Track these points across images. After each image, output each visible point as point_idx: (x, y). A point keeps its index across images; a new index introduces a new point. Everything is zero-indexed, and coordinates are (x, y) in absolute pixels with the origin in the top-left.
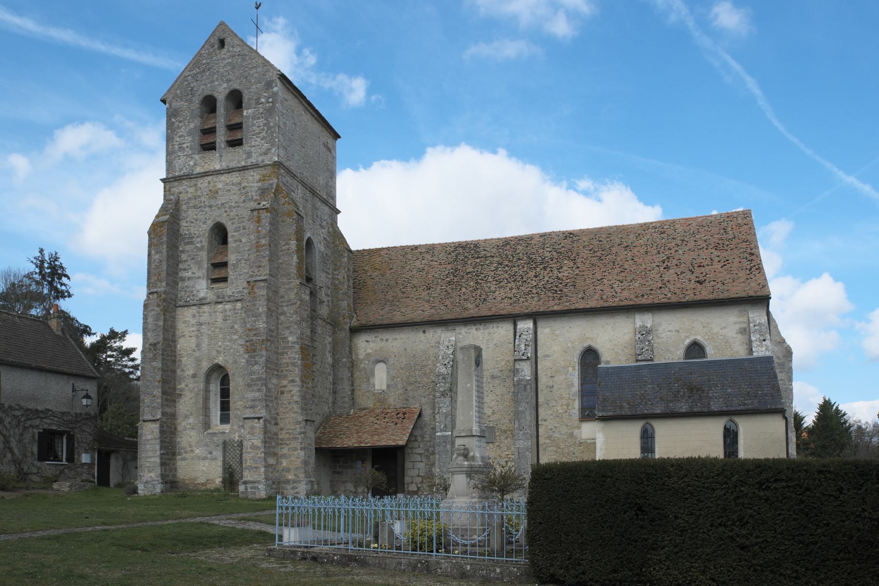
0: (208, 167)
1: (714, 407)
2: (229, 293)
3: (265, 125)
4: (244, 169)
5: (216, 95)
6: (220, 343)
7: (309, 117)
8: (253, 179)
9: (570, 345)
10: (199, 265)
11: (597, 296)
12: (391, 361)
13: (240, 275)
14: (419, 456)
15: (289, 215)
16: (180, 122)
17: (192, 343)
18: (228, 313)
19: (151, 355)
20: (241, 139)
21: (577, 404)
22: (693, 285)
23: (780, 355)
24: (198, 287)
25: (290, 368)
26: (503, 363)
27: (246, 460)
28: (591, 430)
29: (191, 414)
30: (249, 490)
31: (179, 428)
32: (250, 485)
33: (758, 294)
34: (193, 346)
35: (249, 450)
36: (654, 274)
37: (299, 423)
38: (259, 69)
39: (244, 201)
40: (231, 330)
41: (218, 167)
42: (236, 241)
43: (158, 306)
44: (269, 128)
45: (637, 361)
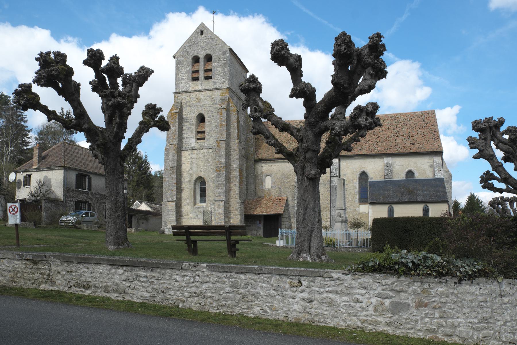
1: (419, 200)
2: (206, 145)
3: (222, 70)
4: (213, 90)
5: (199, 56)
7: (238, 65)
8: (217, 95)
10: (191, 132)
11: (367, 149)
12: (273, 175)
15: (234, 111)
18: (206, 154)
19: (171, 172)
20: (211, 76)
21: (358, 197)
22: (409, 145)
23: (447, 177)
24: (191, 142)
25: (234, 179)
28: (364, 208)
31: (183, 205)
33: (438, 150)
34: (189, 168)
36: (392, 139)
37: (238, 203)
38: (220, 46)
41: (200, 88)
43: (174, 150)
44: (225, 72)
45: (385, 178)
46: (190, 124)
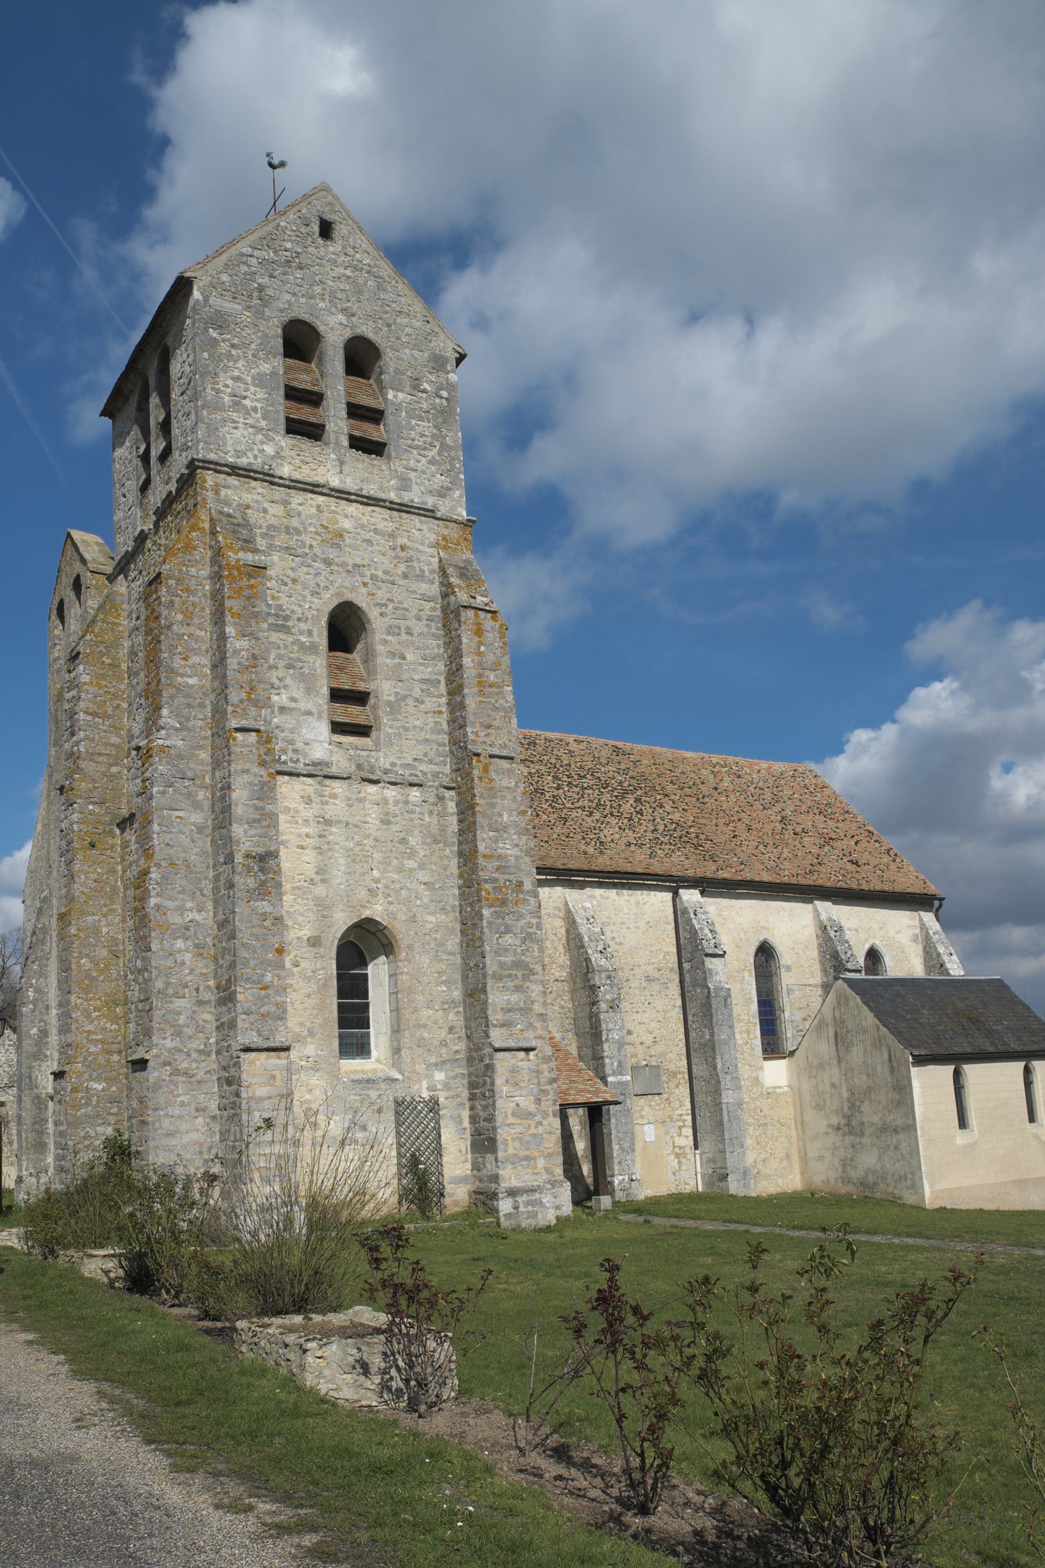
0: (305, 474)
4: (403, 508)
9: (742, 935)
13: (406, 729)
16: (233, 346)
19: (251, 883)
20: (383, 445)
24: (306, 733)
30: (522, 1209)
34: (310, 871)
39: (405, 576)
40: (402, 848)
41: (335, 482)
44: (444, 447)
46: (301, 645)
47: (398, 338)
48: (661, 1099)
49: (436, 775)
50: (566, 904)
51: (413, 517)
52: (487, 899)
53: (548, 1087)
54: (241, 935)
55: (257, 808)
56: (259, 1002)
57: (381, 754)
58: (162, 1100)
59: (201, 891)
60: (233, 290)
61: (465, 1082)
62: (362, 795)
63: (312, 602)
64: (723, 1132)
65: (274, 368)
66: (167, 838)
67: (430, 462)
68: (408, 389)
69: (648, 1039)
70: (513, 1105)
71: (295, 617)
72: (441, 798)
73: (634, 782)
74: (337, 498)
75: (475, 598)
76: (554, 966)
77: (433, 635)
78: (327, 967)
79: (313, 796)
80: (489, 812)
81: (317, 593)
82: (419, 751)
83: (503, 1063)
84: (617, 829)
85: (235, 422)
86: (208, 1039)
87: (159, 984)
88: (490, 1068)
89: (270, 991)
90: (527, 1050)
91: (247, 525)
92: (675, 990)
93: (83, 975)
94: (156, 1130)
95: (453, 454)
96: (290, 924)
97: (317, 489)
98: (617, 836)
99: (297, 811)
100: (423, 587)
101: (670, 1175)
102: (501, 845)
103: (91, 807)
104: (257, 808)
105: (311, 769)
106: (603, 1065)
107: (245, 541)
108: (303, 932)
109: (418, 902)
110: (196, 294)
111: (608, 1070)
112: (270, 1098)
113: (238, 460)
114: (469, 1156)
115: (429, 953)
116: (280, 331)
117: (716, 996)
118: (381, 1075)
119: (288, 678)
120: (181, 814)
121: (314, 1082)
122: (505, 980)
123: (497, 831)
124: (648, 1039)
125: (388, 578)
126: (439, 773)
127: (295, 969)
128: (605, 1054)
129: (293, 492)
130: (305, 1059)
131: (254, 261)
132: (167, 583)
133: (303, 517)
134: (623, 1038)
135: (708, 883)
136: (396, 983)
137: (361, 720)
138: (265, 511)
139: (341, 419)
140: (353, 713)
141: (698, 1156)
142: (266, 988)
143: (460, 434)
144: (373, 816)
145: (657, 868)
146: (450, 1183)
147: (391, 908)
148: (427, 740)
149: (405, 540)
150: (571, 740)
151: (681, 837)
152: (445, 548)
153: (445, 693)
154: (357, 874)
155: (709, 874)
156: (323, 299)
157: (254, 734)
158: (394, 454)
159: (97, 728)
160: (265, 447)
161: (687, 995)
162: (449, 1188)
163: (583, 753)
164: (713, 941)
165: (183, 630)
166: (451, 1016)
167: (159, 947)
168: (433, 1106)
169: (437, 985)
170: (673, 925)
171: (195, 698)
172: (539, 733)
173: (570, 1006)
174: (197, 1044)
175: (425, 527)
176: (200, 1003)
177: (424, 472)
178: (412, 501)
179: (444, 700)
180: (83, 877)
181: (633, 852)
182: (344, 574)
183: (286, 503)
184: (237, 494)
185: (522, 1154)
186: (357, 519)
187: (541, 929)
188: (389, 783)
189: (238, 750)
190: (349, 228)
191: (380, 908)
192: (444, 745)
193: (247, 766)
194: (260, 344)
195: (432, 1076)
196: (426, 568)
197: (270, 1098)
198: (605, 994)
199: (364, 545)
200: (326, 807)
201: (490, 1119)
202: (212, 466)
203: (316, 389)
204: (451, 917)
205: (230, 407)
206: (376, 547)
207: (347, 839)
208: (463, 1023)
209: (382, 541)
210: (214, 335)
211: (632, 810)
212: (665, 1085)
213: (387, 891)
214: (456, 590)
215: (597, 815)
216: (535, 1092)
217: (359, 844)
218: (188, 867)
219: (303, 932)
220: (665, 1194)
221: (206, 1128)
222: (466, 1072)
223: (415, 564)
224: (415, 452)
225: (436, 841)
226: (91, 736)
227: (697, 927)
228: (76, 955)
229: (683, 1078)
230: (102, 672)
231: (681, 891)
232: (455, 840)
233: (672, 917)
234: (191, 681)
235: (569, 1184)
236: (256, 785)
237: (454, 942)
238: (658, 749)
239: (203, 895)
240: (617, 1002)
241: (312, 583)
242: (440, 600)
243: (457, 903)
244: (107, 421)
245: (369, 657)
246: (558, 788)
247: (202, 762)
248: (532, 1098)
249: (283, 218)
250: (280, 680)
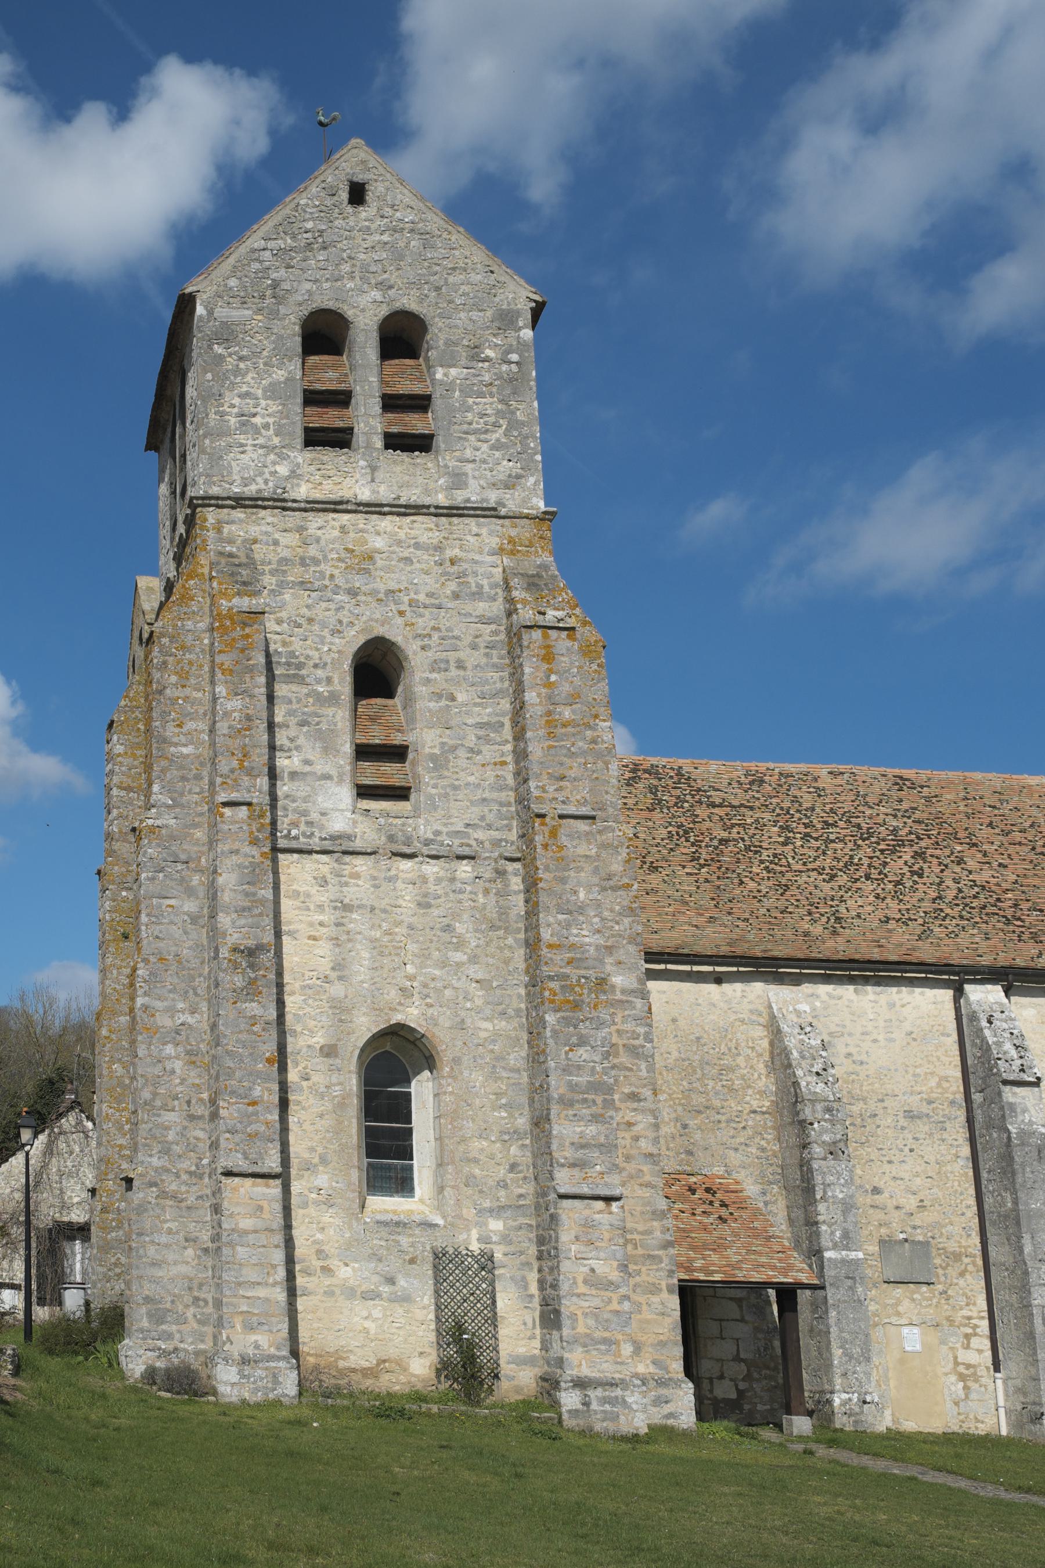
0: (328, 491)
4: (453, 512)
6: (410, 969)
10: (327, 742)
13: (456, 788)
14: (733, 1306)
16: (241, 359)
17: (322, 956)
18: (432, 887)
19: (239, 981)
20: (430, 437)
24: (323, 801)
26: (933, 1082)
27: (573, 1317)
29: (323, 1160)
30: (594, 1406)
32: (599, 1392)
34: (325, 966)
35: (582, 1289)
39: (456, 596)
40: (446, 937)
41: (365, 494)
42: (439, 696)
43: (254, 842)
44: (514, 424)
46: (319, 698)
47: (450, 302)
48: (932, 1291)
49: (496, 843)
50: (770, 1007)
51: (467, 520)
52: (552, 1002)
53: (660, 1253)
54: (225, 1042)
55: (247, 894)
56: (245, 1119)
57: (421, 821)
58: (148, 1226)
59: (194, 989)
60: (242, 294)
61: (533, 1235)
62: (393, 872)
63: (331, 643)
64: (1035, 1349)
65: (290, 372)
66: (156, 930)
67: (493, 448)
68: (464, 362)
69: (911, 1203)
70: (586, 1269)
71: (311, 663)
72: (501, 873)
73: (920, 829)
74: (366, 513)
75: (544, 614)
76: (750, 1092)
77: (494, 665)
78: (349, 1083)
79: (329, 876)
80: (558, 888)
81: (339, 632)
82: (473, 814)
83: (571, 1213)
84: (871, 898)
85: (242, 445)
86: (201, 1159)
87: (146, 1095)
88: (554, 1218)
89: (259, 1108)
90: (608, 1199)
91: (251, 563)
92: (958, 1133)
93: (115, 1082)
94: (140, 1257)
95: (526, 430)
96: (299, 1029)
97: (340, 507)
98: (870, 908)
99: (308, 895)
100: (482, 607)
101: (949, 1405)
102: (575, 931)
103: (124, 894)
104: (247, 894)
105: (327, 845)
106: (818, 1234)
107: (244, 583)
108: (315, 1040)
109: (468, 1005)
110: (200, 310)
111: (825, 1241)
112: (256, 1232)
113: (246, 489)
114: (538, 1331)
115: (482, 1068)
116: (297, 328)
117: (1023, 1144)
118: (417, 1218)
119: (302, 737)
120: (172, 902)
121: (326, 1219)
122: (577, 1106)
123: (570, 913)
124: (911, 1203)
125: (433, 601)
126: (501, 840)
127: (305, 1084)
128: (820, 1218)
129: (310, 515)
130: (315, 1191)
131: (268, 253)
132: (160, 642)
133: (323, 543)
134: (852, 1197)
135: (1015, 974)
136: (439, 1105)
137: (396, 781)
138: (276, 543)
139: (373, 417)
140: (387, 773)
141: (999, 1383)
142: (254, 1103)
143: (536, 404)
144: (407, 898)
145: (927, 953)
146: (509, 1363)
147: (430, 1011)
148: (484, 800)
149: (457, 552)
150: (824, 772)
151: (984, 907)
152: (512, 553)
153: (510, 738)
154: (386, 970)
155: (1020, 962)
156: (353, 278)
157: (244, 808)
158: (443, 446)
159: (131, 804)
160: (278, 468)
161: (979, 1141)
162: (506, 1368)
163: (839, 790)
164: (1019, 1062)
165: (179, 693)
166: (514, 1150)
167: (146, 1052)
168: (487, 1263)
169: (494, 1110)
170: (955, 1036)
171: (190, 770)
172: (771, 765)
173: (776, 1148)
174: (186, 1165)
175: (484, 531)
176: (192, 1118)
177: (484, 462)
178: (468, 500)
179: (509, 747)
180: (115, 972)
181: (890, 931)
182: (374, 604)
183: (300, 530)
184: (241, 527)
185: (598, 1334)
186: (392, 535)
187: (651, 1041)
188: (429, 856)
189: (226, 827)
190: (387, 184)
191: (416, 1012)
192: (509, 804)
193: (236, 845)
194: (274, 349)
195: (486, 1225)
196: (485, 582)
197: (256, 1232)
198: (821, 1133)
199: (401, 565)
200: (345, 889)
201: (555, 1286)
202: (213, 502)
203: (342, 387)
204: (515, 1023)
205: (237, 429)
206: (418, 566)
207: (372, 927)
208: (530, 1160)
209: (425, 557)
210: (220, 351)
211: (906, 869)
212: (940, 1271)
213: (425, 991)
214: (519, 606)
215: (843, 879)
216: (619, 1256)
217: (388, 933)
218: (179, 962)
219: (315, 1040)
220: (940, 1431)
221: (196, 1261)
222: (534, 1223)
223: (470, 579)
224: (472, 438)
225: (493, 927)
226: (125, 813)
227: (991, 1040)
228: (107, 1059)
229: (974, 1264)
230: (137, 740)
231: (968, 987)
232: (521, 925)
233: (953, 1025)
234: (185, 750)
235: (691, 1385)
236: (247, 868)
237: (518, 1056)
238: (978, 776)
239: (196, 994)
240: (841, 1145)
241: (333, 621)
242: (504, 621)
243: (523, 1006)
244: (153, 455)
245: (409, 702)
246: (785, 844)
247: (197, 842)
248: (615, 1264)
249: (304, 195)
250: (292, 740)
